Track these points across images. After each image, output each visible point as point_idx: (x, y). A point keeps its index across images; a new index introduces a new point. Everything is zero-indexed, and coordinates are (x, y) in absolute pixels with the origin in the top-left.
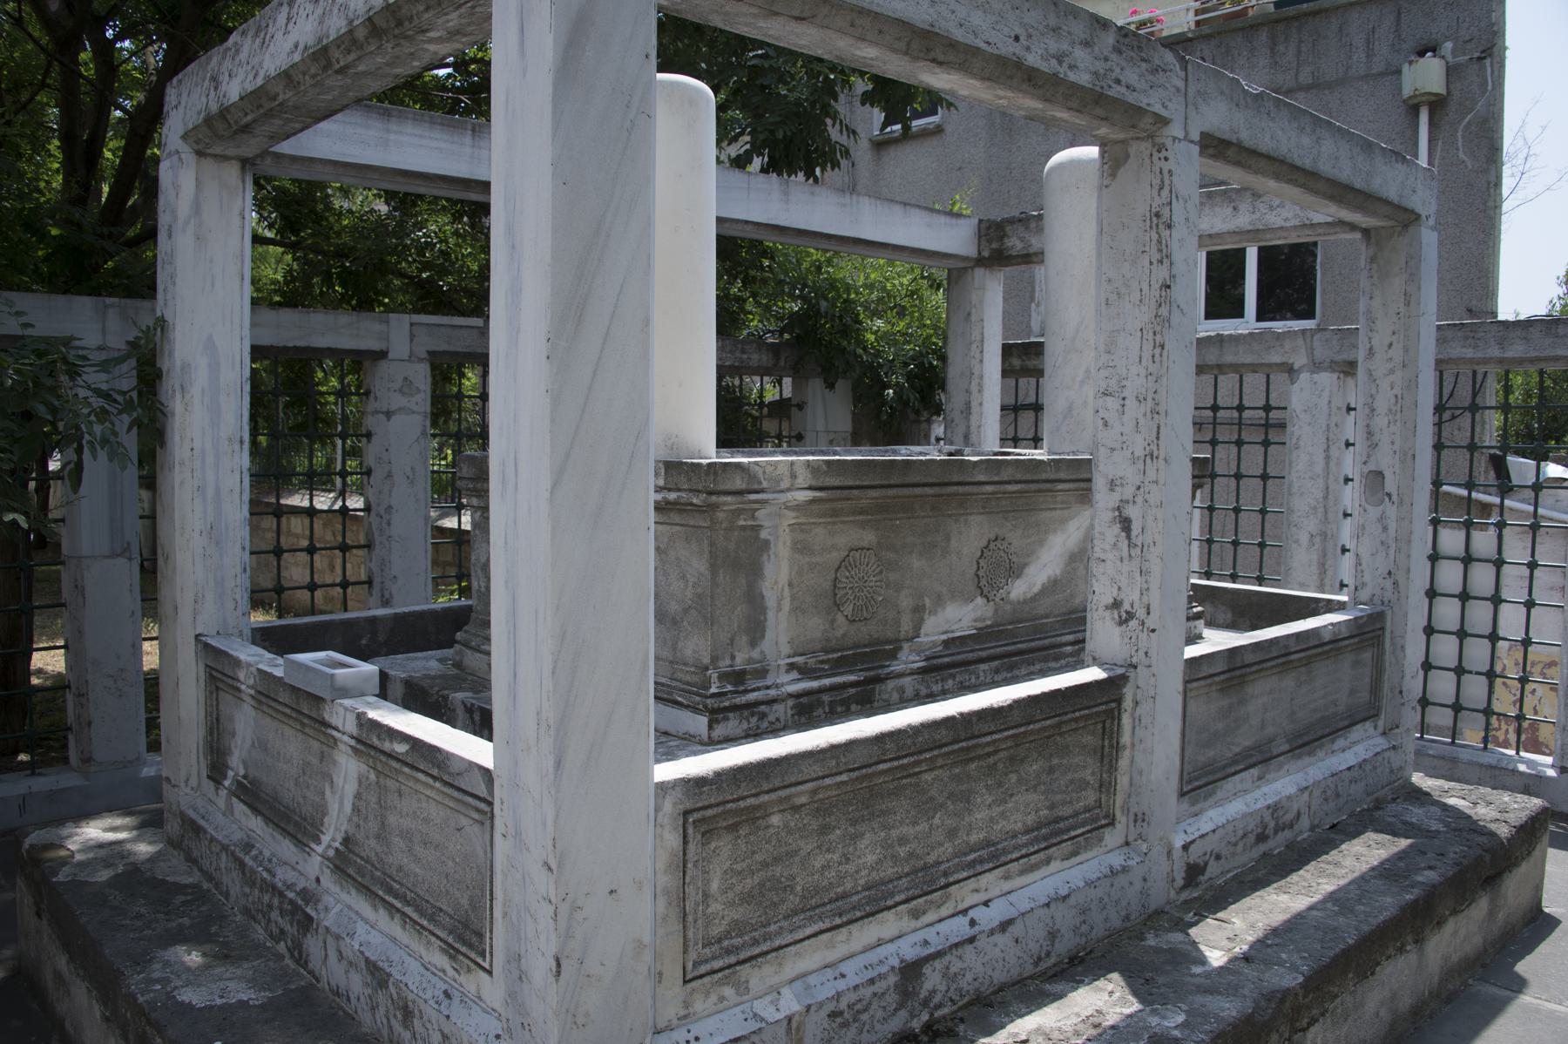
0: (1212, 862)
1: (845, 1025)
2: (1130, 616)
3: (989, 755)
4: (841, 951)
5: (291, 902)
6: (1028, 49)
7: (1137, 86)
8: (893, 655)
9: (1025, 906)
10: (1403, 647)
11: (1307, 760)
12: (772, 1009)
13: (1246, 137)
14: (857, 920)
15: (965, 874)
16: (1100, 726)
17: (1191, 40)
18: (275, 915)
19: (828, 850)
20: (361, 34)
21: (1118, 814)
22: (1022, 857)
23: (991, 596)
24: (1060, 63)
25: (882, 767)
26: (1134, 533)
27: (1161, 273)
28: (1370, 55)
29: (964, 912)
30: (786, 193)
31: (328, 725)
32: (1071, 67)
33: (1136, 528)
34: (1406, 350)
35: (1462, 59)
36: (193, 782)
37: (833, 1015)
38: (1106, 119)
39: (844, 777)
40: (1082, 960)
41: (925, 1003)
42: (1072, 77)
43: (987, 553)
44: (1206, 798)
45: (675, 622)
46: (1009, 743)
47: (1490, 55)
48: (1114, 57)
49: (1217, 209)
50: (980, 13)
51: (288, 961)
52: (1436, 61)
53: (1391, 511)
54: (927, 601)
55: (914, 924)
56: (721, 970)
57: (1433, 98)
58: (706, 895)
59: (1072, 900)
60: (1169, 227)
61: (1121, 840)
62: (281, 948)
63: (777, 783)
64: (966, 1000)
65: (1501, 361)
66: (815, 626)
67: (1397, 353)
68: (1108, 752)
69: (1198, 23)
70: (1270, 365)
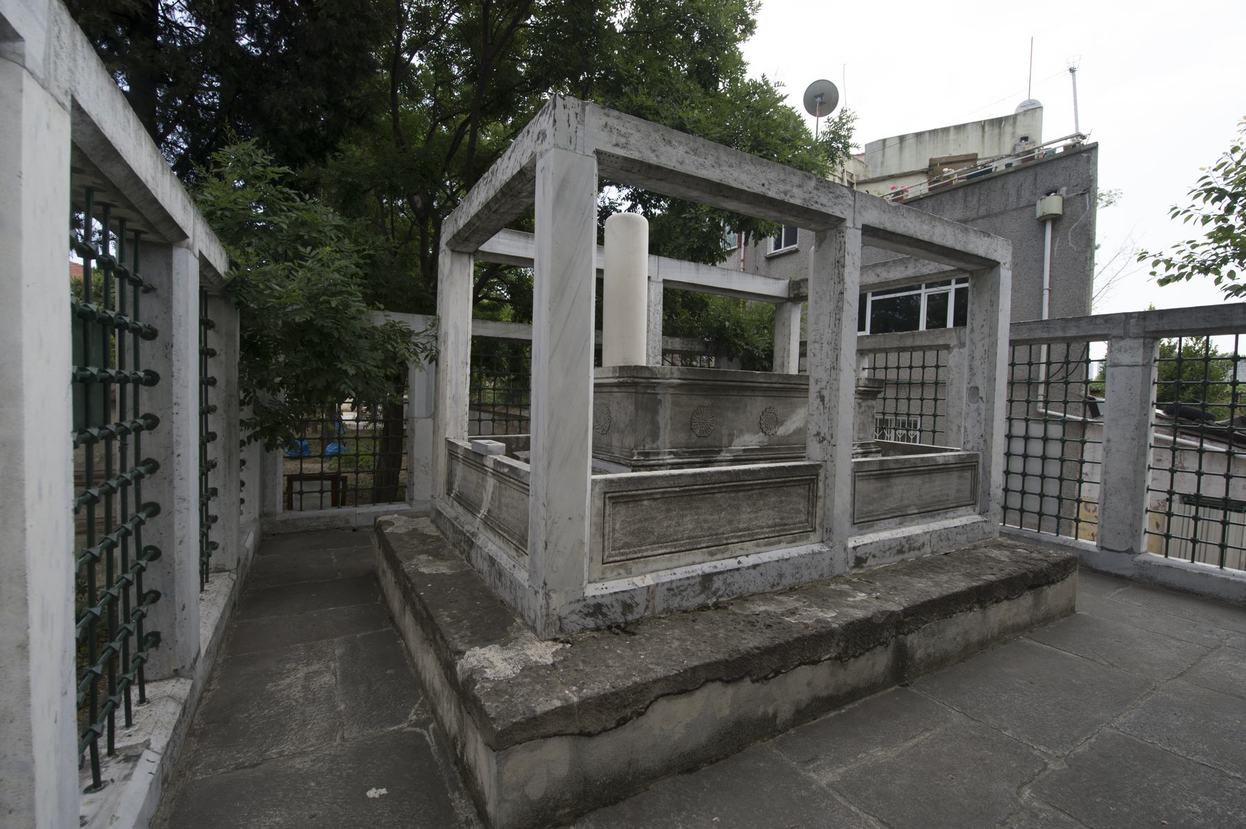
0: (870, 557)
1: (675, 595)
2: (824, 439)
3: (748, 490)
4: (675, 563)
5: (468, 537)
6: (769, 189)
7: (827, 204)
8: (719, 452)
9: (766, 560)
10: (990, 472)
11: (929, 519)
12: (641, 582)
13: (889, 226)
14: (683, 551)
15: (736, 541)
16: (807, 486)
17: (922, 199)
18: (462, 544)
19: (670, 520)
20: (499, 196)
21: (817, 527)
22: (766, 538)
23: (767, 432)
24: (786, 195)
25: (695, 487)
26: (826, 402)
27: (839, 288)
28: (1019, 196)
29: (736, 557)
30: (698, 270)
31: (484, 465)
32: (791, 197)
33: (826, 399)
34: (991, 328)
35: (1071, 195)
36: (441, 496)
37: (669, 590)
38: (811, 220)
39: (677, 489)
40: (796, 590)
41: (715, 593)
42: (792, 201)
43: (765, 414)
44: (867, 528)
45: (623, 432)
46: (759, 487)
47: (1089, 192)
48: (815, 192)
49: (898, 268)
50: (745, 175)
51: (465, 562)
52: (1057, 197)
53: (983, 406)
54: (735, 432)
55: (710, 558)
56: (619, 561)
57: (1054, 216)
58: (614, 530)
59: (791, 562)
60: (844, 267)
61: (820, 539)
62: (464, 557)
63: (646, 487)
64: (735, 596)
65: (1063, 339)
66: (682, 437)
67: (986, 330)
68: (812, 499)
69: (930, 189)
70: (938, 346)
